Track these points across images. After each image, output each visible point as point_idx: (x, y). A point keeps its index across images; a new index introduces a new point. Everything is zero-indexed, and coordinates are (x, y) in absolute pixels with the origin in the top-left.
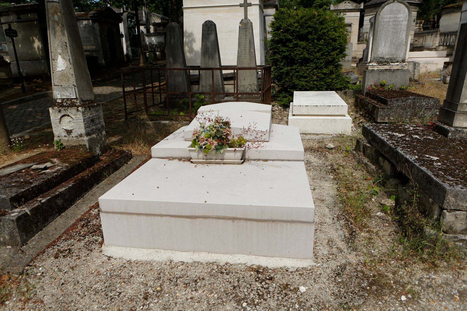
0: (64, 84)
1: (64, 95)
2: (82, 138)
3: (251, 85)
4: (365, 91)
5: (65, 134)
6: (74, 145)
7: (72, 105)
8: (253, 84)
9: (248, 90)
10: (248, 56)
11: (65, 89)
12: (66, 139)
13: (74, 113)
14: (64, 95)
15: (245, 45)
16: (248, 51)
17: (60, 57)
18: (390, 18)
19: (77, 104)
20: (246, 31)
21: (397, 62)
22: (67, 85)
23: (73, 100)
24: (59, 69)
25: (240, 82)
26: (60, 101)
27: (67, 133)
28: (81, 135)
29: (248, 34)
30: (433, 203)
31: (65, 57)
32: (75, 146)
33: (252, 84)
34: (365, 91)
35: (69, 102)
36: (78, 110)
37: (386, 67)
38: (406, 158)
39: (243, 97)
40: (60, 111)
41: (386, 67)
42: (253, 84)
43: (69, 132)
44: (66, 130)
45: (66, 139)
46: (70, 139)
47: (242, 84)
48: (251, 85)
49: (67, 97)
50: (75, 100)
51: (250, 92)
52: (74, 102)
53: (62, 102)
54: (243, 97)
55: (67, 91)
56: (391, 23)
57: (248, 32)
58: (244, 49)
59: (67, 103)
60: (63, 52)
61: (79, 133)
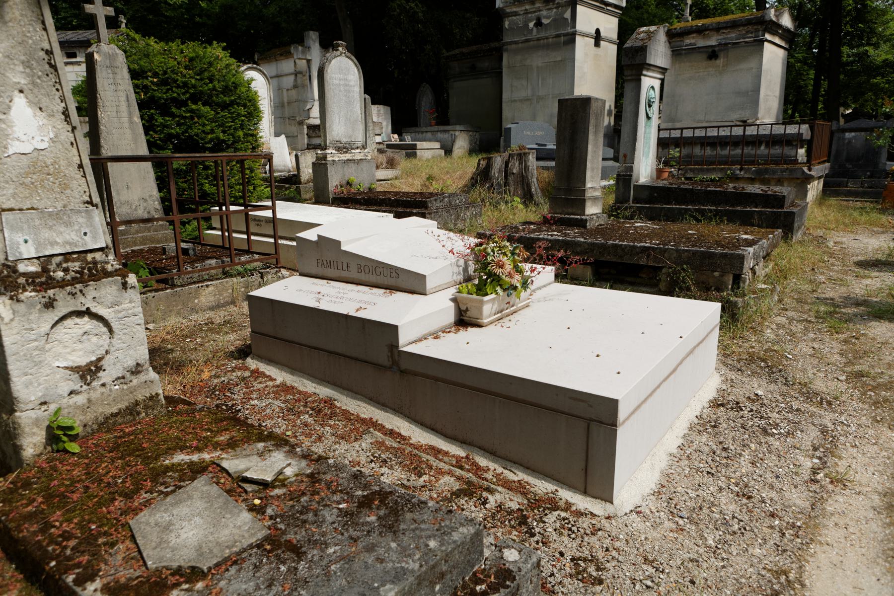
0: (47, 202)
1: (53, 243)
2: (142, 377)
3: (145, 200)
4: (331, 196)
5: (75, 383)
6: (115, 410)
7: (92, 273)
8: (150, 196)
9: (141, 213)
10: (128, 131)
11: (60, 217)
12: (80, 399)
13: (110, 299)
14: (53, 243)
15: (118, 106)
16: (125, 120)
17: (20, 102)
18: (340, 80)
19: (109, 268)
20: (114, 73)
21: (358, 148)
22: (59, 206)
23: (89, 257)
24: (15, 147)
25: (118, 194)
26: (33, 268)
27: (83, 377)
28: (137, 370)
29: (120, 82)
30: (722, 276)
31: (45, 102)
32: (117, 414)
33: (146, 196)
34: (331, 196)
35: (75, 266)
36: (125, 285)
37: (348, 156)
38: (762, 228)
39: (133, 230)
40: (50, 305)
41: (348, 156)
42: (150, 196)
43: (88, 372)
44: (75, 369)
45: (80, 399)
46: (95, 395)
47: (123, 198)
48: (145, 200)
49: (69, 249)
50: (98, 256)
51: (146, 216)
52: (95, 262)
53: (45, 270)
54: (133, 230)
55: (68, 224)
56: (342, 89)
57: (119, 77)
58: (114, 114)
59: (66, 270)
60: (34, 83)
61: (131, 363)
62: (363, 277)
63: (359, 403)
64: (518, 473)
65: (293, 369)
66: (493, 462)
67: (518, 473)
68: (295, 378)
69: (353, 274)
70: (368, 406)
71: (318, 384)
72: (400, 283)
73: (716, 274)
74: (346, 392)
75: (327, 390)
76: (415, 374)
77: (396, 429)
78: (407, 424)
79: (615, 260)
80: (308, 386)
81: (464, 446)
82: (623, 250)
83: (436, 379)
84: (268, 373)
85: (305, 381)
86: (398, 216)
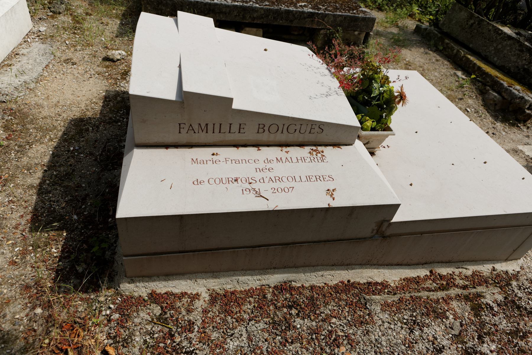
62: (265, 137)
63: (320, 273)
64: (468, 267)
65: (214, 272)
66: (448, 267)
67: (468, 267)
68: (223, 280)
69: (250, 135)
70: (333, 272)
71: (261, 274)
72: (323, 138)
73: (356, 33)
74: (300, 269)
75: (276, 276)
76: (400, 235)
77: (370, 280)
78: (376, 271)
79: (286, 24)
80: (251, 282)
81: (426, 266)
82: (294, 15)
83: (422, 233)
84: (176, 291)
85: (241, 278)
86: (219, 24)
